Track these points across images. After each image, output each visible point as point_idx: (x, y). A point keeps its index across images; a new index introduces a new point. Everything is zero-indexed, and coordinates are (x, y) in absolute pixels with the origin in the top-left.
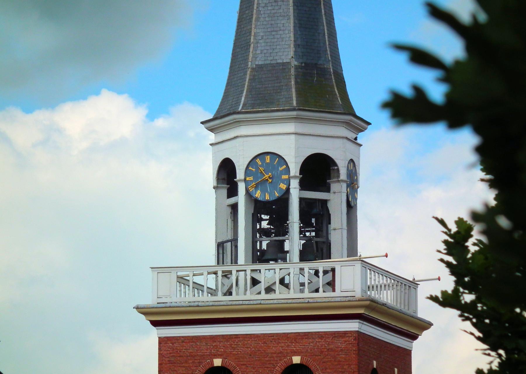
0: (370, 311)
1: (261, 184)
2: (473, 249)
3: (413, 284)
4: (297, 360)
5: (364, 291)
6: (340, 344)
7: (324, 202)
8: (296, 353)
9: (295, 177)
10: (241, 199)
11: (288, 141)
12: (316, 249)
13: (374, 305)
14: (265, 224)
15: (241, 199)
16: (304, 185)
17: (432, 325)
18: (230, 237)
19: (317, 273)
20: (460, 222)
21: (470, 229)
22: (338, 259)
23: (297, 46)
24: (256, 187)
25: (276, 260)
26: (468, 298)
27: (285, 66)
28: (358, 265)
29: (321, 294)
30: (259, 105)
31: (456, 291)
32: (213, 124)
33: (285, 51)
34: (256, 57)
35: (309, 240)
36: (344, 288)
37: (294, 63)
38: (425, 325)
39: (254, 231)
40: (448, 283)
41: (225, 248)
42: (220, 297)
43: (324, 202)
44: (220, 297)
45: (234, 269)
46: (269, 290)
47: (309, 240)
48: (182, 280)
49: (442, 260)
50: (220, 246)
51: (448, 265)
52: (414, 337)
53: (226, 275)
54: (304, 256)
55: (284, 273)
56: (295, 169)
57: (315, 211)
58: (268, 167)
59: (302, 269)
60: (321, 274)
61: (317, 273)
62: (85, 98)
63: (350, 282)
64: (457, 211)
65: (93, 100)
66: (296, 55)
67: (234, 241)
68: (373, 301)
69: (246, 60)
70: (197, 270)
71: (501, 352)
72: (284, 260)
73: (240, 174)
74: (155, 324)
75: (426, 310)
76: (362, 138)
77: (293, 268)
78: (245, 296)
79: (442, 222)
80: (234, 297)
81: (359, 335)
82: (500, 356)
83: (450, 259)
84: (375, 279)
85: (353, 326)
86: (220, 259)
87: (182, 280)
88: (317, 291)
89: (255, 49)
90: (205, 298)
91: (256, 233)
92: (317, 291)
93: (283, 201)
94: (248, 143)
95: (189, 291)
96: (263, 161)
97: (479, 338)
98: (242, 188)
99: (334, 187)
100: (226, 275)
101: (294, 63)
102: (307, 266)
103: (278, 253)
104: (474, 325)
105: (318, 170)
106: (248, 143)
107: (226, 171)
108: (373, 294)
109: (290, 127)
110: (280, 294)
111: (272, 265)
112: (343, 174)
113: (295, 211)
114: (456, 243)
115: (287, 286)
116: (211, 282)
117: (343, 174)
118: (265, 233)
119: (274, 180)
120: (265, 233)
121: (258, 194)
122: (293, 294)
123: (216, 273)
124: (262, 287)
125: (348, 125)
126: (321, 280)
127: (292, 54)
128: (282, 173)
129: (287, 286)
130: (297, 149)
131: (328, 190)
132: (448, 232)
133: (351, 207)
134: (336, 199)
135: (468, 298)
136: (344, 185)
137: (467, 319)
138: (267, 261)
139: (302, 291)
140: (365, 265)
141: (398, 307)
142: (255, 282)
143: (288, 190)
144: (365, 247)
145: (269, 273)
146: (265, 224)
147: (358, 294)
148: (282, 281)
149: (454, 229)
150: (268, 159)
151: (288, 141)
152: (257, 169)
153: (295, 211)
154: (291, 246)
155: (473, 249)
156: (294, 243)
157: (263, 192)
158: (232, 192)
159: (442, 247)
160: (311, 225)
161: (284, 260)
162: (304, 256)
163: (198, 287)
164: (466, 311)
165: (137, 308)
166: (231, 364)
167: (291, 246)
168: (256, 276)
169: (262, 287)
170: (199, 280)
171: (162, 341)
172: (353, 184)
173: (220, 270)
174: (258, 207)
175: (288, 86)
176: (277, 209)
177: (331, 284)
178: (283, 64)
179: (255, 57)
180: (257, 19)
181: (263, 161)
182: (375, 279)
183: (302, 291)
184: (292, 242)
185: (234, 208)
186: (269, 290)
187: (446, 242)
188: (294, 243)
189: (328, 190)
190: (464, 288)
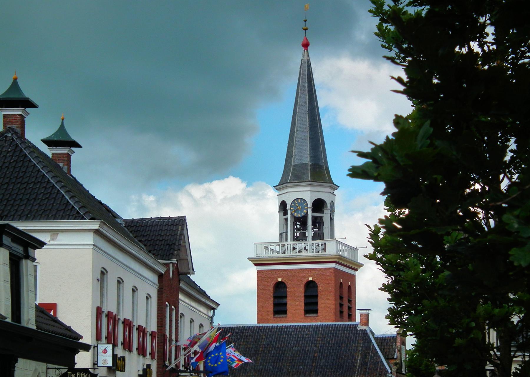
0: (339, 260)
1: (297, 210)
2: (381, 236)
3: (356, 249)
4: (311, 279)
5: (337, 252)
6: (328, 273)
7: (321, 217)
8: (310, 276)
9: (310, 208)
10: (289, 216)
11: (307, 193)
12: (318, 236)
13: (341, 257)
14: (298, 226)
15: (289, 216)
16: (314, 211)
17: (363, 265)
18: (284, 231)
19: (318, 245)
20: (376, 226)
21: (380, 229)
22: (326, 240)
23: (311, 157)
24: (295, 212)
25: (302, 240)
26: (379, 256)
27: (306, 164)
28: (335, 242)
29: (320, 253)
30: (296, 180)
31: (374, 253)
32: (278, 187)
33: (306, 159)
34: (295, 161)
35: (315, 232)
36: (329, 251)
37: (310, 163)
38: (361, 265)
39: (294, 229)
40: (371, 250)
41: (282, 236)
42: (281, 254)
43: (321, 217)
44: (281, 254)
45: (286, 243)
46: (300, 252)
47: (315, 232)
48: (266, 248)
49: (369, 241)
50: (281, 234)
51: (371, 243)
52: (357, 270)
53: (283, 246)
54: (314, 238)
55: (305, 245)
56: (310, 205)
57: (318, 221)
58: (299, 204)
59: (313, 244)
60: (320, 245)
61: (318, 245)
62: (223, 179)
63: (331, 249)
64: (374, 222)
65: (226, 179)
66: (310, 160)
67: (286, 233)
68: (340, 256)
69: (291, 162)
70: (272, 244)
71: (392, 277)
72: (306, 240)
73: (288, 207)
74: (256, 265)
75: (361, 260)
76: (336, 192)
77: (309, 243)
78: (290, 254)
79: (369, 226)
80: (286, 254)
81: (335, 269)
82: (392, 278)
83: (372, 241)
84: (341, 247)
85: (333, 265)
86: (281, 240)
87: (266, 248)
88: (319, 252)
89: (294, 158)
90: (275, 255)
91: (295, 229)
92: (319, 252)
93: (305, 217)
94: (291, 195)
95: (269, 252)
96: (298, 201)
97: (383, 271)
98: (289, 212)
99: (325, 211)
100: (283, 246)
101: (310, 163)
102: (314, 242)
103: (303, 237)
104: (382, 266)
105: (319, 205)
106: (291, 195)
107: (283, 206)
108: (341, 253)
109: (308, 188)
110: (304, 253)
111: (301, 242)
112: (329, 207)
113: (310, 220)
114: (374, 234)
115: (307, 250)
116: (277, 248)
117: (329, 207)
118: (298, 229)
119: (302, 209)
120: (298, 229)
121: (295, 215)
122: (309, 253)
123: (279, 245)
124: (297, 250)
125: (331, 187)
126: (320, 248)
127: (309, 160)
128: (305, 206)
129: (307, 250)
130: (311, 197)
131: (323, 213)
132: (371, 230)
133: (332, 219)
134: (326, 216)
135: (379, 256)
136: (329, 211)
137: (379, 264)
138: (299, 240)
139: (313, 252)
140: (337, 241)
141: (350, 258)
142: (294, 249)
143: (307, 212)
144: (337, 235)
145: (300, 245)
146: (298, 226)
147: (335, 253)
148: (305, 248)
149: (373, 229)
150: (299, 201)
151: (307, 193)
152: (295, 204)
153: (310, 220)
154: (309, 234)
155: (381, 236)
156: (309, 233)
157: (298, 214)
158: (286, 213)
159: (369, 236)
160: (316, 226)
161: (306, 240)
162: (314, 238)
163: (272, 250)
164: (379, 261)
165: (249, 259)
166: (285, 281)
167: (309, 234)
168: (295, 246)
169: (297, 250)
170: (272, 248)
171: (258, 272)
172: (332, 210)
173: (281, 244)
174: (296, 220)
175: (307, 172)
176: (303, 221)
177: (324, 249)
178: (305, 164)
179: (294, 161)
180: (295, 147)
181: (298, 201)
182: (341, 247)
183: (313, 252)
184: (309, 233)
185: (286, 220)
186: (300, 252)
187: (370, 234)
188: (309, 233)
189: (323, 213)
190: (490, 363)
